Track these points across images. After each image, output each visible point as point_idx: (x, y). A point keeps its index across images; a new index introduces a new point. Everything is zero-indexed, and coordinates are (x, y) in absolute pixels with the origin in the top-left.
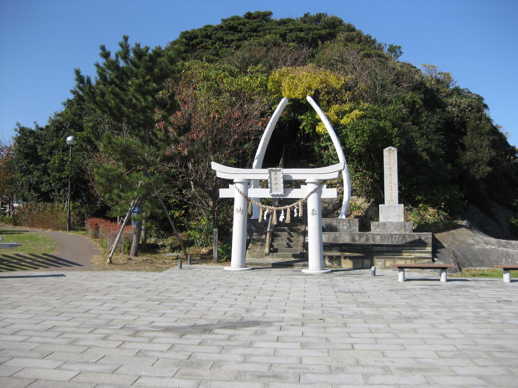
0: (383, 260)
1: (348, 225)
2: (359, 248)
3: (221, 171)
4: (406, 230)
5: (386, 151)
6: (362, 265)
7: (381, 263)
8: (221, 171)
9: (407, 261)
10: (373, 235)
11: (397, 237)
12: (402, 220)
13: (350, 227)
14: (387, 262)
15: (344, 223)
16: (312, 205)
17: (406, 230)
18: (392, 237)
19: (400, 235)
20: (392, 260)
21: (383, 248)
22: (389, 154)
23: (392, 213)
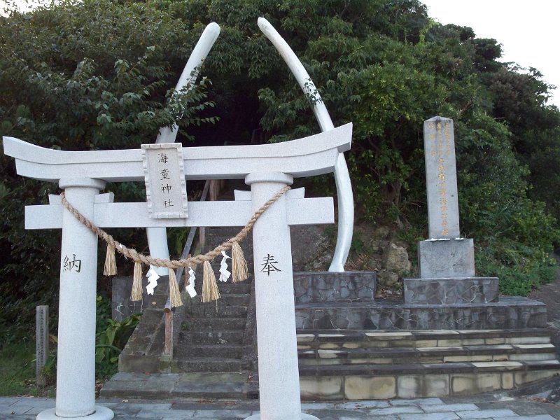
0: (447, 377)
1: (351, 287)
2: (384, 344)
3: (32, 160)
4: (482, 298)
5: (429, 126)
6: (397, 391)
7: (441, 385)
8: (32, 160)
9: (505, 376)
10: (412, 310)
11: (467, 313)
12: (471, 273)
13: (355, 290)
14: (456, 381)
15: (343, 284)
16: (273, 245)
17: (482, 298)
18: (455, 314)
19: (474, 310)
20: (470, 375)
21: (441, 342)
22: (437, 130)
23: (446, 254)
